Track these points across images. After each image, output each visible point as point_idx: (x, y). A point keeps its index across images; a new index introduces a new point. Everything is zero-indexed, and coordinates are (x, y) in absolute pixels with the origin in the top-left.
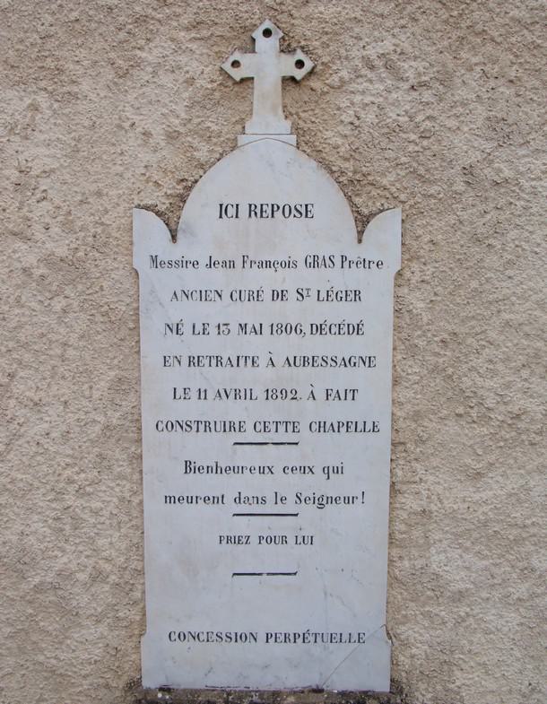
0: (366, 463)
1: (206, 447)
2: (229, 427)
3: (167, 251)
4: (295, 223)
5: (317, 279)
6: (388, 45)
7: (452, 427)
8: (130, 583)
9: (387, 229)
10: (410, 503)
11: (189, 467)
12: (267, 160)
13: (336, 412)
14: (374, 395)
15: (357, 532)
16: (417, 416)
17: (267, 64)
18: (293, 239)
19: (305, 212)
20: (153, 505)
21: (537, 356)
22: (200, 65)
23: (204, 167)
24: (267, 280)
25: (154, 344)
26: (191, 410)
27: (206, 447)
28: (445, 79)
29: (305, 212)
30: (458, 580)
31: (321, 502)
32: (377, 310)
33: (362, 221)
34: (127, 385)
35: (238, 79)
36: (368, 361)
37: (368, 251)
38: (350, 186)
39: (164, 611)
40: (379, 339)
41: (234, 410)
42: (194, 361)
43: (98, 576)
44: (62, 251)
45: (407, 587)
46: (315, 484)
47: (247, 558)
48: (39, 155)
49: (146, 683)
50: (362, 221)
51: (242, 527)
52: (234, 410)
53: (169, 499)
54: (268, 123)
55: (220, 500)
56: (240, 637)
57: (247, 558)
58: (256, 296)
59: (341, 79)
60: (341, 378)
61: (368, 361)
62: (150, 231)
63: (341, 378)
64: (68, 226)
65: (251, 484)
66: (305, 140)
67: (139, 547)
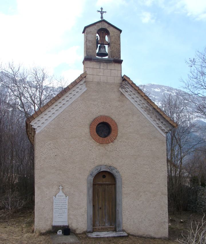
0: (66, 211)
1: (57, 210)
2: (59, 208)
3: (55, 198)
4: (62, 197)
5: (63, 200)
6: (67, 186)
7: (72, 209)
8: (52, 219)
9: (68, 197)
10: (69, 213)
11: (56, 211)
12: (61, 193)
13: (64, 207)
14: (67, 207)
15: (66, 215)
16: (69, 208)
17: (61, 188)
18: (62, 198)
19: (63, 196)
20: (54, 213)
21: (167, 212)
22: (57, 188)
23: (57, 193)
24: (61, 200)
25: (54, 204)
26: (56, 208)
27: (57, 210)
28: (71, 188)
29: (63, 196)
30: (72, 218)
31: (64, 213)
32: (67, 200)
33: (66, 197)
34: (53, 206)
35: (34, 124)
36: (66, 205)
37: (66, 198)
38: (65, 195)
39: (54, 220)
40: (67, 203)
41: (58, 207)
42: (56, 205)
43: (50, 218)
44: (49, 198)
45: (69, 218)
46: (63, 212)
47: (59, 217)
48: (47, 193)
49: (53, 225)
50: (66, 197)
51: (59, 215)
52: (58, 207)
53: (55, 213)
54: (61, 191)
55: (58, 213)
56: (59, 222)
57: (59, 217)
58: (60, 201)
59: (63, 240)
60: (65, 206)
61: (66, 205)
62: (54, 197)
63: (65, 206)
64: (49, 197)
65: (59, 212)
66: (63, 192)
67: (53, 216)
